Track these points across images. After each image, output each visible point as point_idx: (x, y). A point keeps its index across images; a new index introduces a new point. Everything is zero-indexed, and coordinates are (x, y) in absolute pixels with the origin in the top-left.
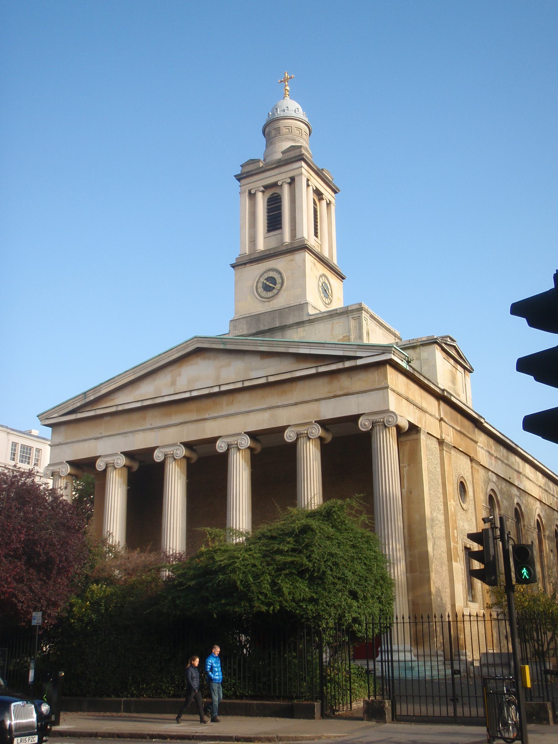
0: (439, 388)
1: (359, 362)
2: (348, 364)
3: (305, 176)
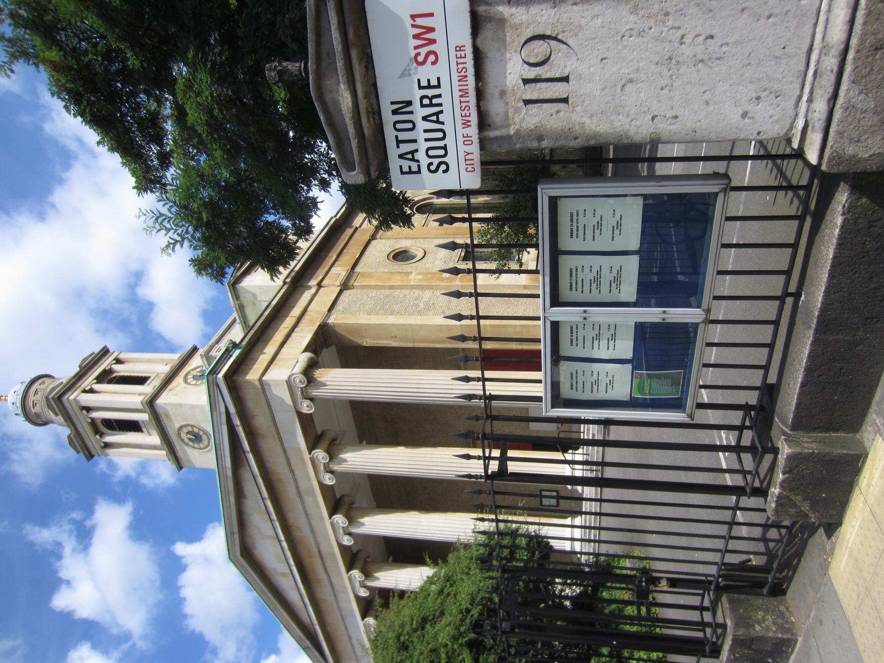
0: (283, 286)
1: (232, 410)
2: (237, 422)
3: (78, 395)
